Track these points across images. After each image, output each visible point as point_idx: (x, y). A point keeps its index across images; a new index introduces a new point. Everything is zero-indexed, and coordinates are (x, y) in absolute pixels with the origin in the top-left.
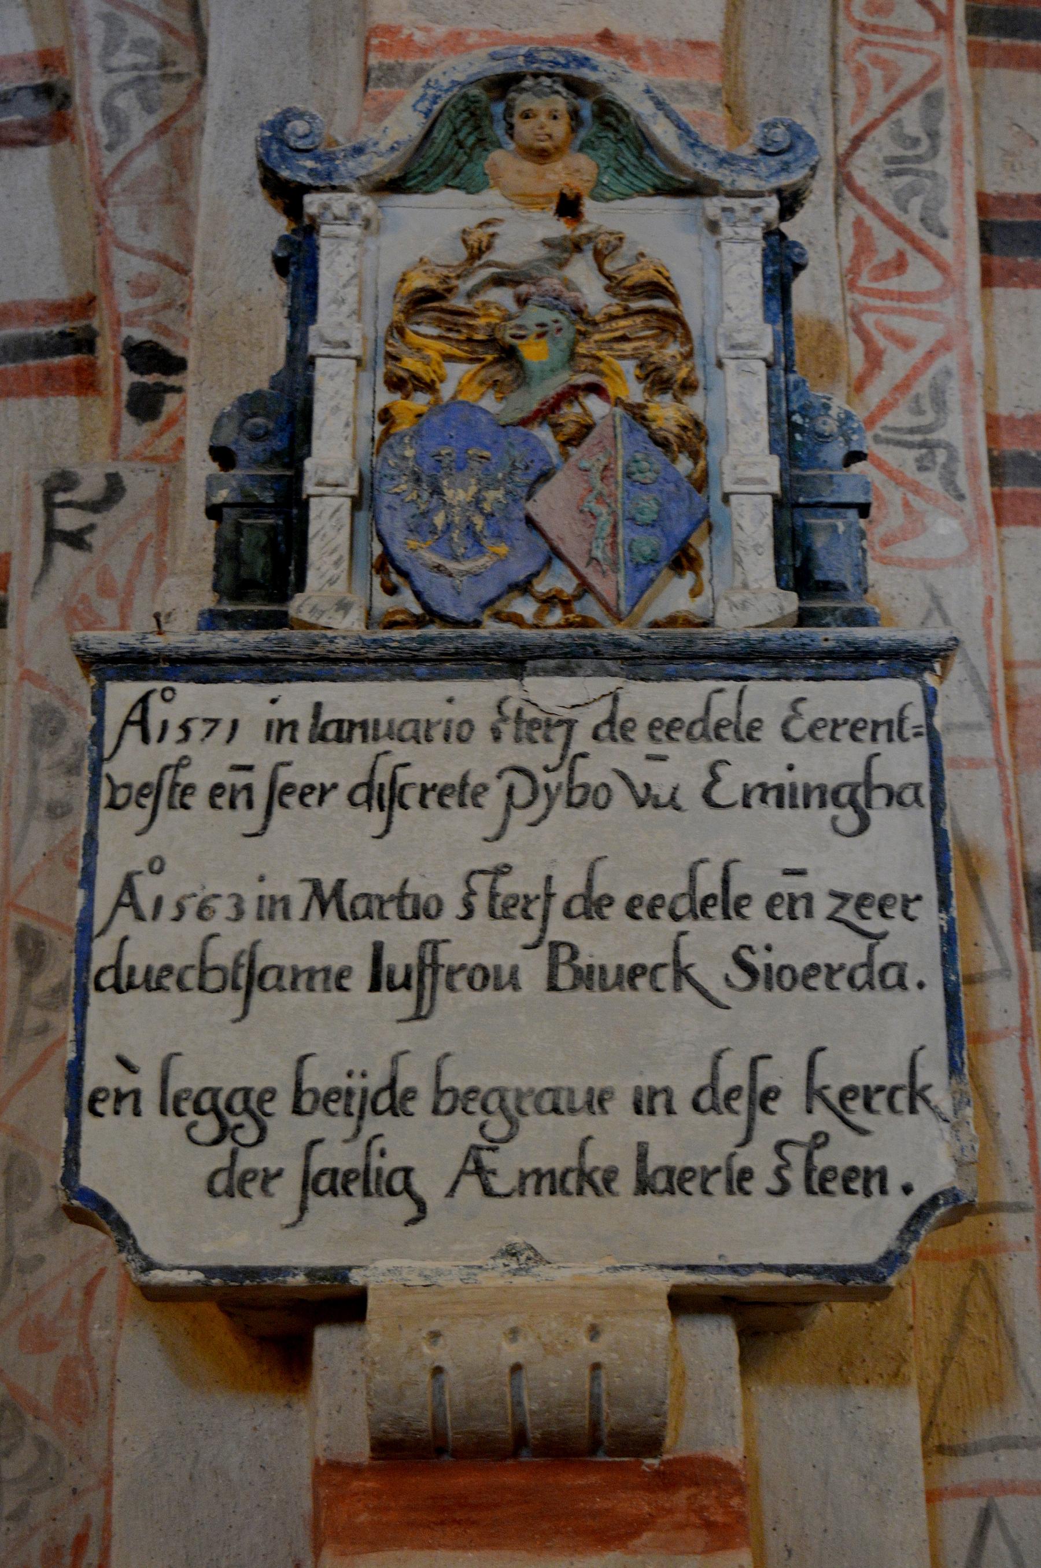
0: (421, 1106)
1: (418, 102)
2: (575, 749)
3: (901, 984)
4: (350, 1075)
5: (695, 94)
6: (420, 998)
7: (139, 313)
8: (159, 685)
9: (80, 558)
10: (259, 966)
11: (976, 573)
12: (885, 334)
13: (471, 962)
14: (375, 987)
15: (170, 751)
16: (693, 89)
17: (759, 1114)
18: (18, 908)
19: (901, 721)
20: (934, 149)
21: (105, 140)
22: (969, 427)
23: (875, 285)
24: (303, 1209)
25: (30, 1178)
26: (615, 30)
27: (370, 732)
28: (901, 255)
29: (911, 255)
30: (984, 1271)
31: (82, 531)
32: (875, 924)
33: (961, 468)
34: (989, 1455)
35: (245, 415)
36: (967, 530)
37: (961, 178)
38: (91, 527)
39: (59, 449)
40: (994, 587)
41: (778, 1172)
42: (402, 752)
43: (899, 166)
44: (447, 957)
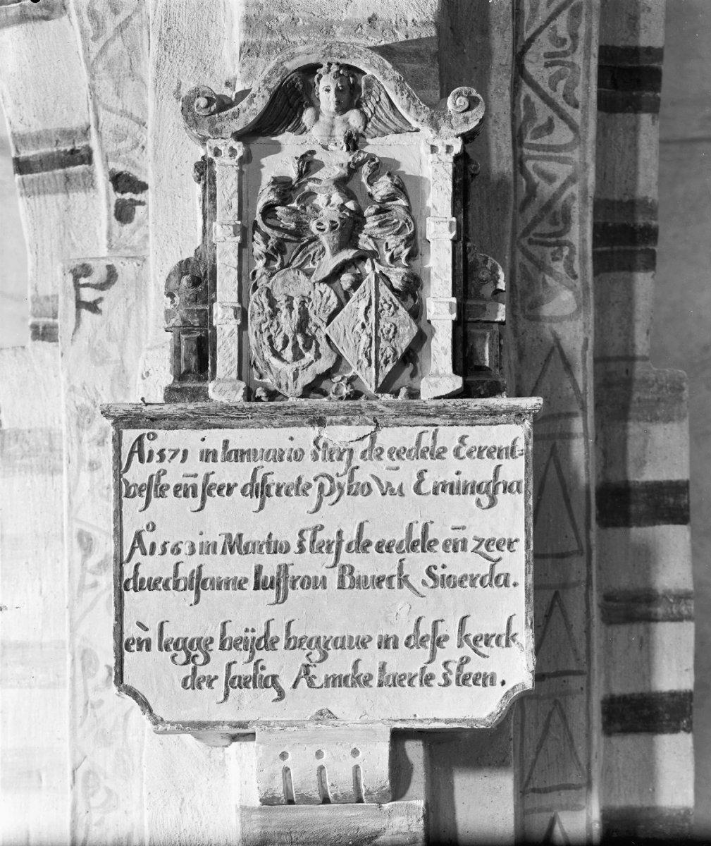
0: (281, 645)
2: (354, 464)
3: (506, 584)
4: (247, 630)
5: (423, 57)
6: (278, 593)
7: (119, 153)
8: (147, 431)
9: (96, 318)
10: (203, 577)
11: (580, 324)
12: (538, 174)
13: (302, 575)
14: (256, 588)
15: (154, 467)
16: (422, 53)
17: (438, 649)
18: (77, 520)
19: (513, 449)
20: (574, 47)
21: (91, 34)
22: (583, 232)
23: (534, 142)
24: (226, 695)
25: (94, 662)
27: (252, 457)
28: (550, 120)
29: (557, 121)
30: (560, 704)
31: (95, 302)
32: (495, 555)
34: (557, 793)
35: (182, 273)
36: (577, 298)
37: (589, 66)
38: (101, 299)
39: (77, 227)
40: (589, 332)
41: (444, 675)
42: (269, 466)
43: (553, 59)
44: (292, 572)
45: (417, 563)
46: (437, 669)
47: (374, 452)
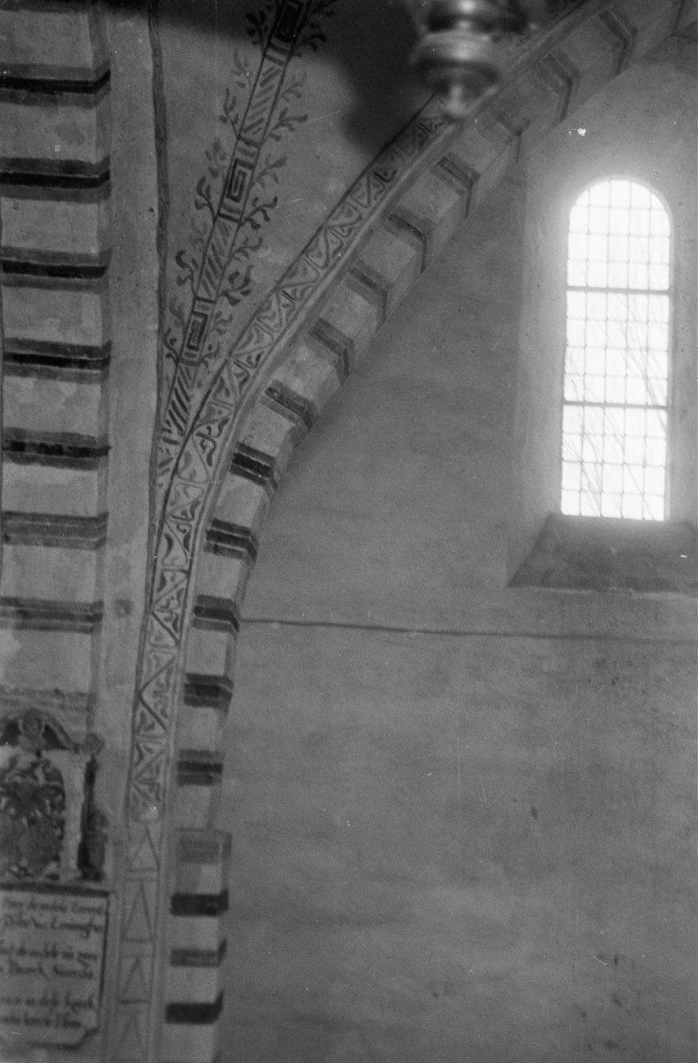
1: (284, 277)
26: (61, 688)
33: (160, 793)
45: (48, 964)
46: (53, 1018)
47: (33, 906)
